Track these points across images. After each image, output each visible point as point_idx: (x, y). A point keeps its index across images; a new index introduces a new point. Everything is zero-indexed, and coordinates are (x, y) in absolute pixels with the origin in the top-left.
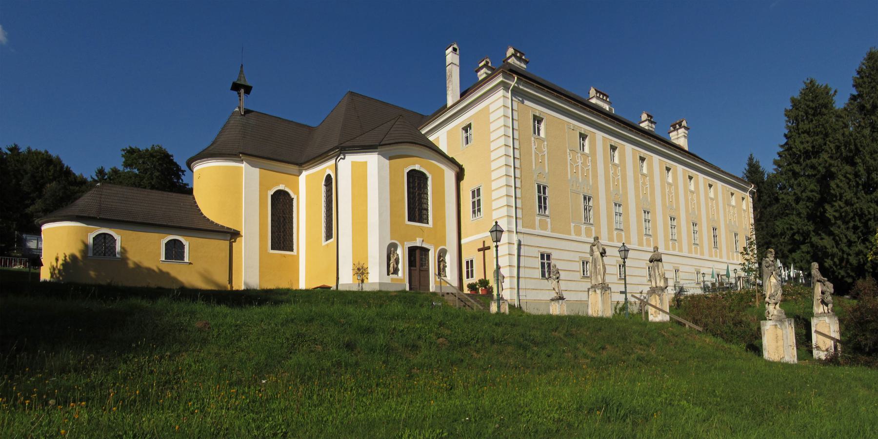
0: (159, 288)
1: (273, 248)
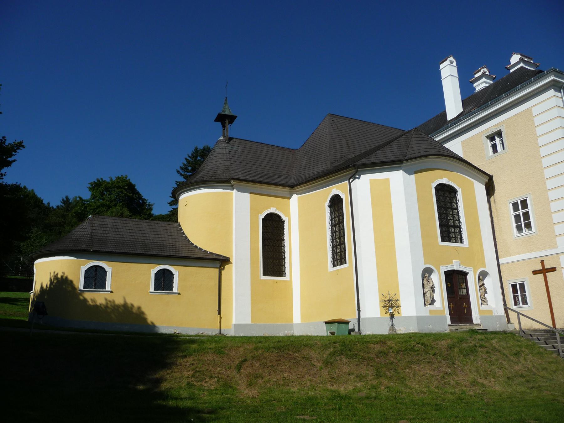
1: (265, 274)
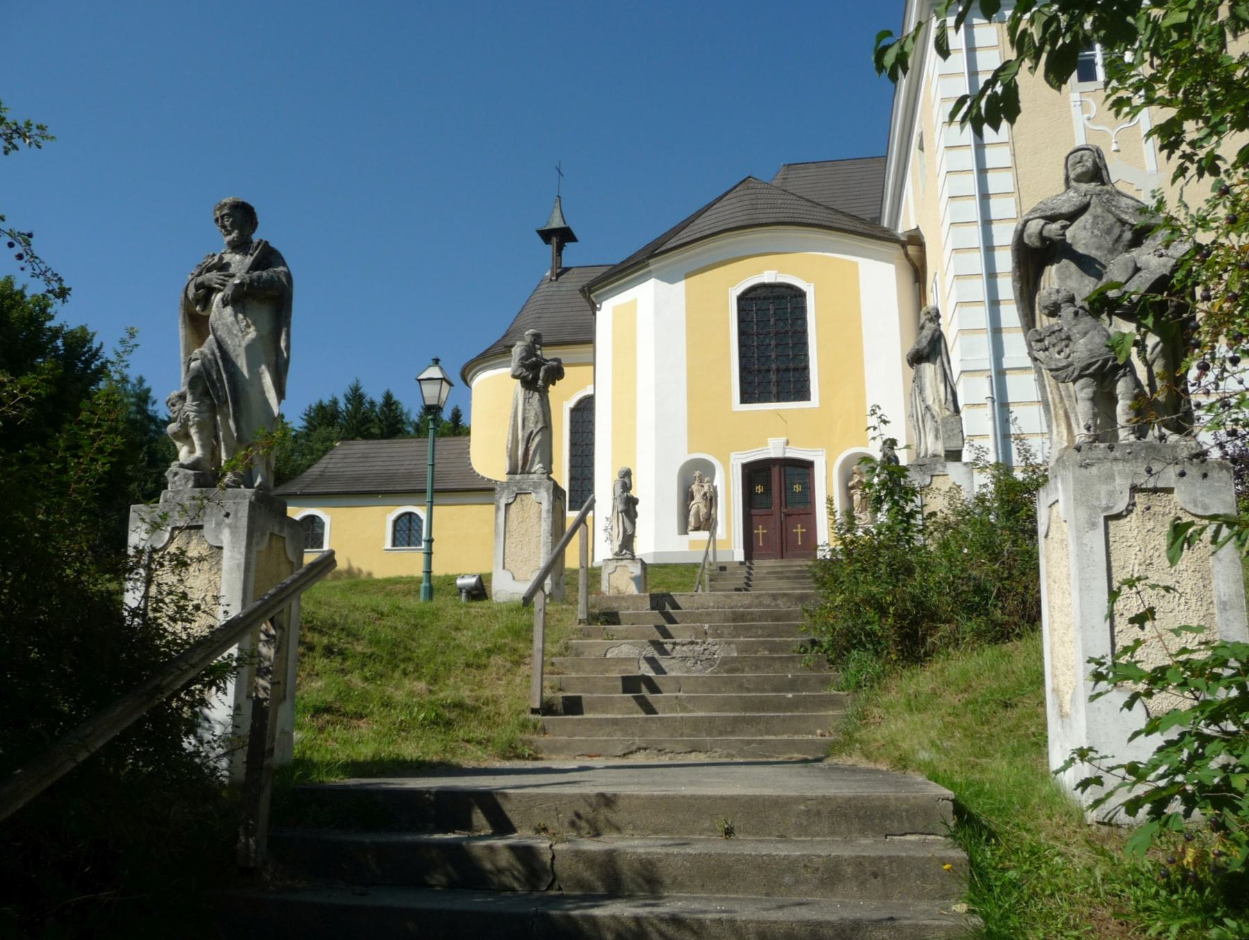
0: (636, 515)
